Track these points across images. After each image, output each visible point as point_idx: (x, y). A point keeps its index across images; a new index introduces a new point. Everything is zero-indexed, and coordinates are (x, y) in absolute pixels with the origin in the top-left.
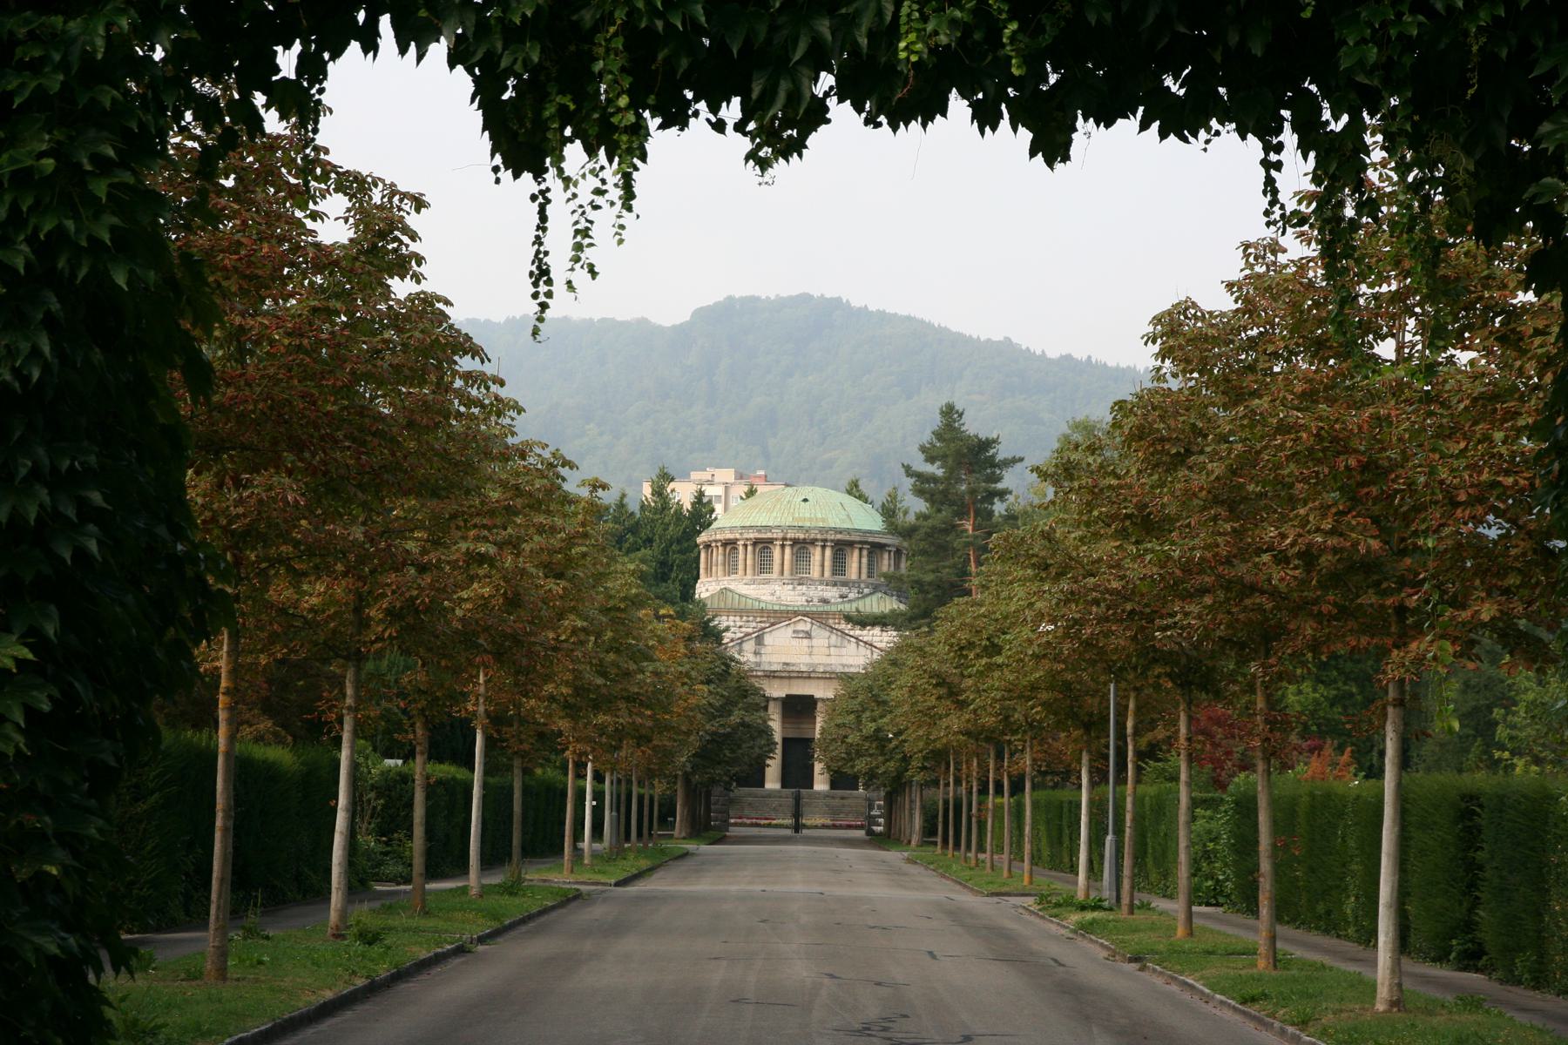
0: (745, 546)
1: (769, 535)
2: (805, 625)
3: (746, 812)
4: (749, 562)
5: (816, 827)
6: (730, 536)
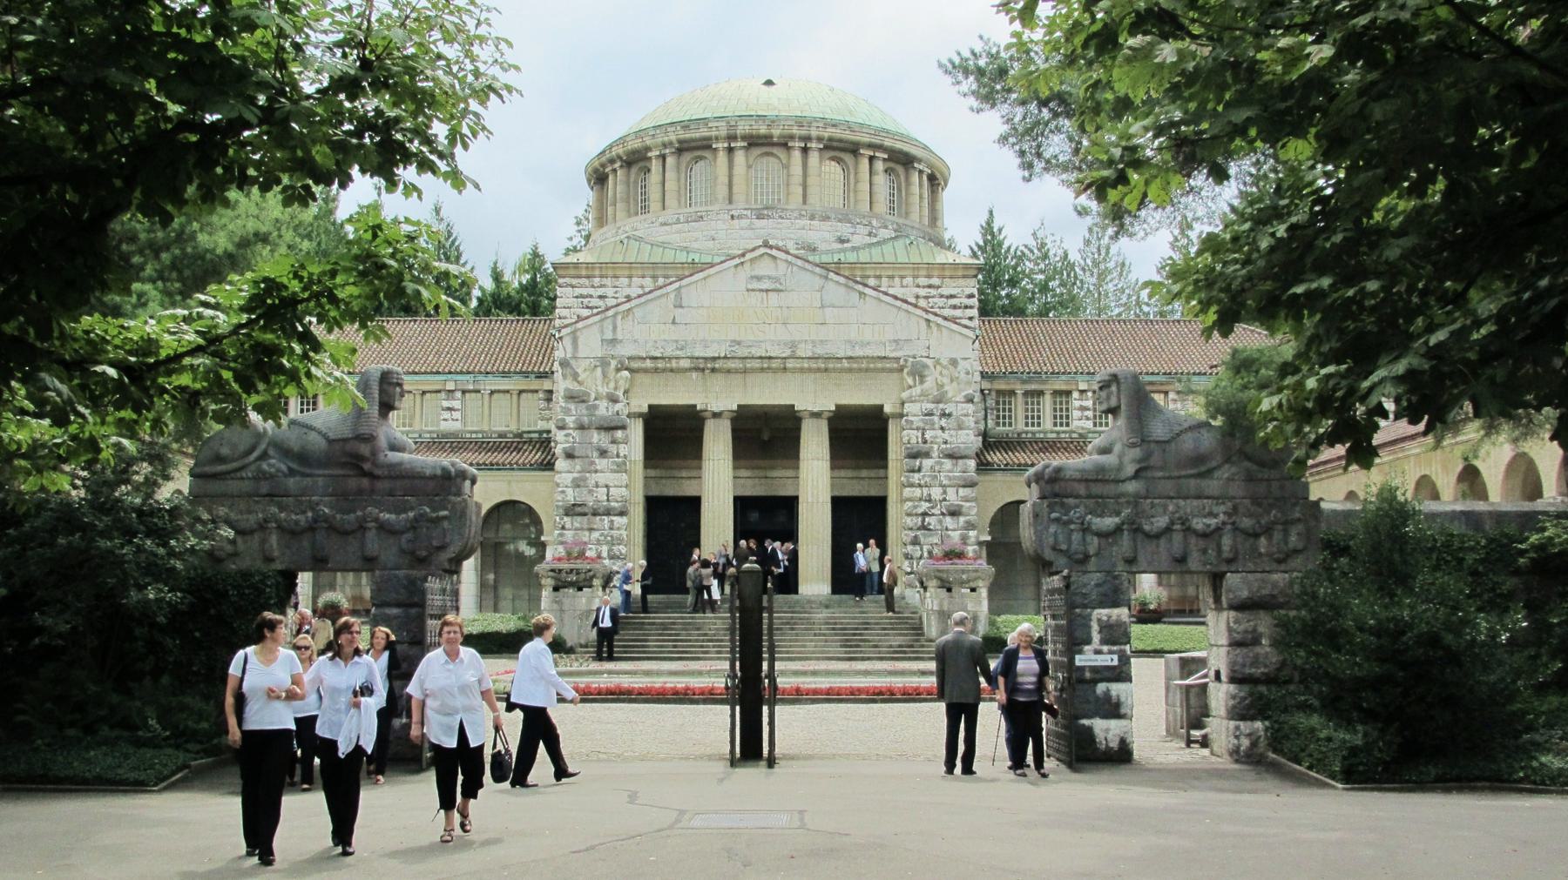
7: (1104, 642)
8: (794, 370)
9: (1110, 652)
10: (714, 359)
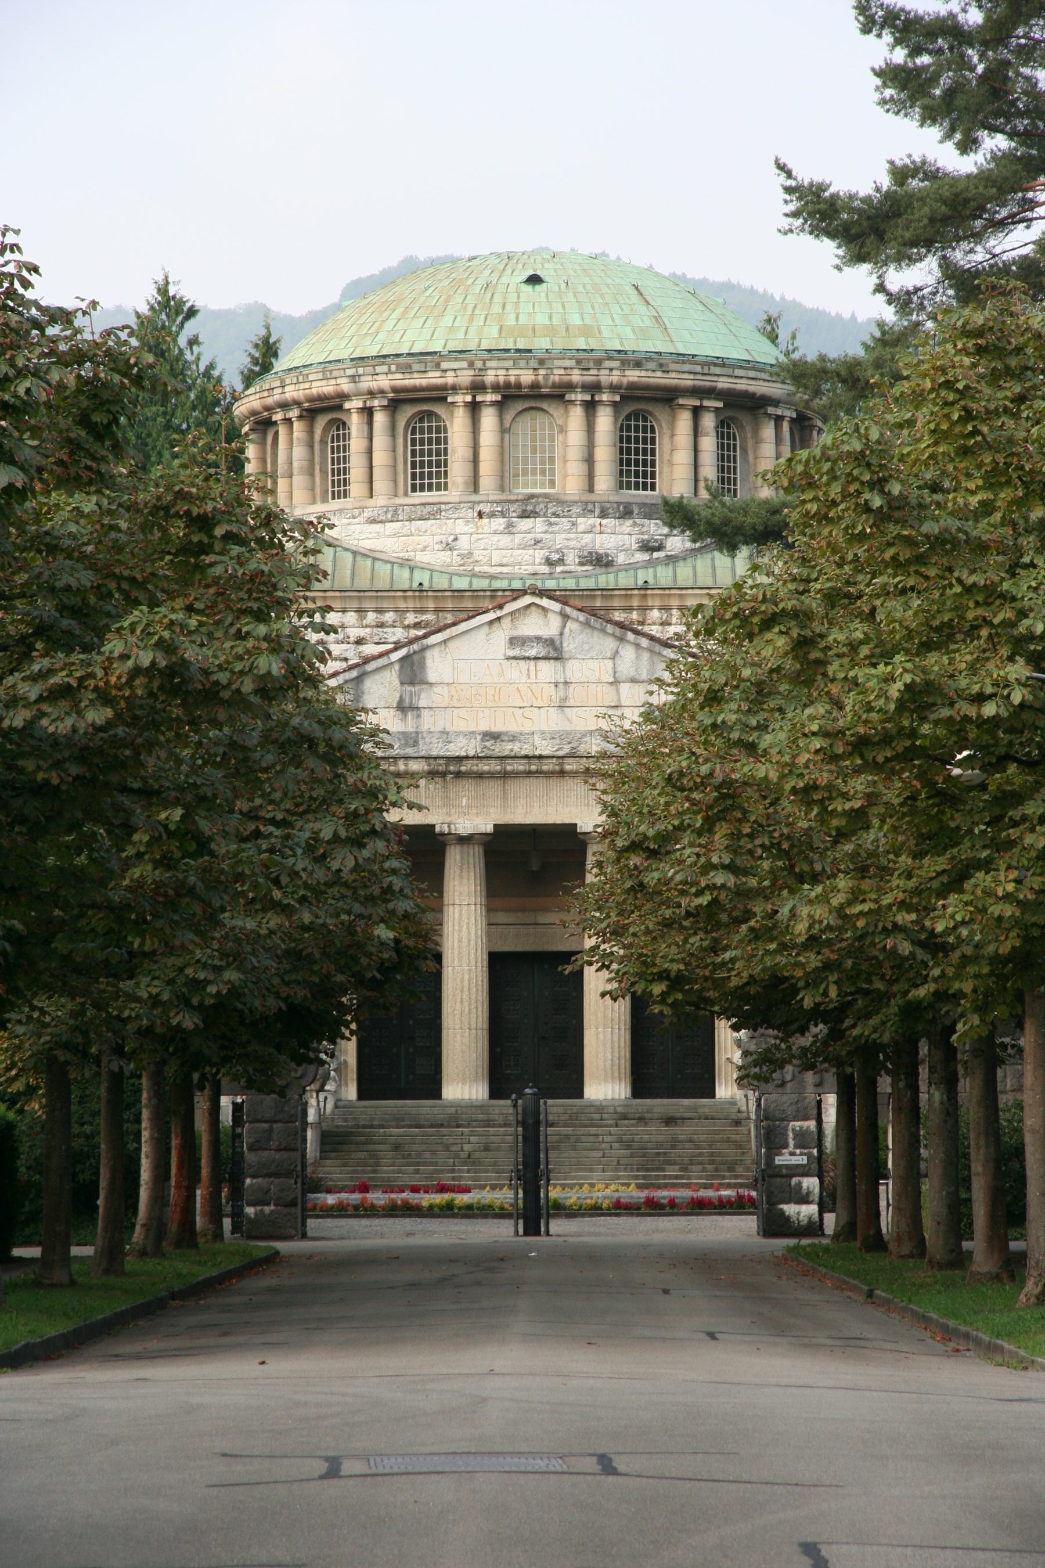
0: (368, 412)
1: (434, 378)
2: (541, 624)
3: (387, 1171)
4: (380, 458)
5: (596, 1210)
6: (327, 388)
7: (796, 1147)
8: (574, 774)
9: (801, 1154)
10: (460, 759)
